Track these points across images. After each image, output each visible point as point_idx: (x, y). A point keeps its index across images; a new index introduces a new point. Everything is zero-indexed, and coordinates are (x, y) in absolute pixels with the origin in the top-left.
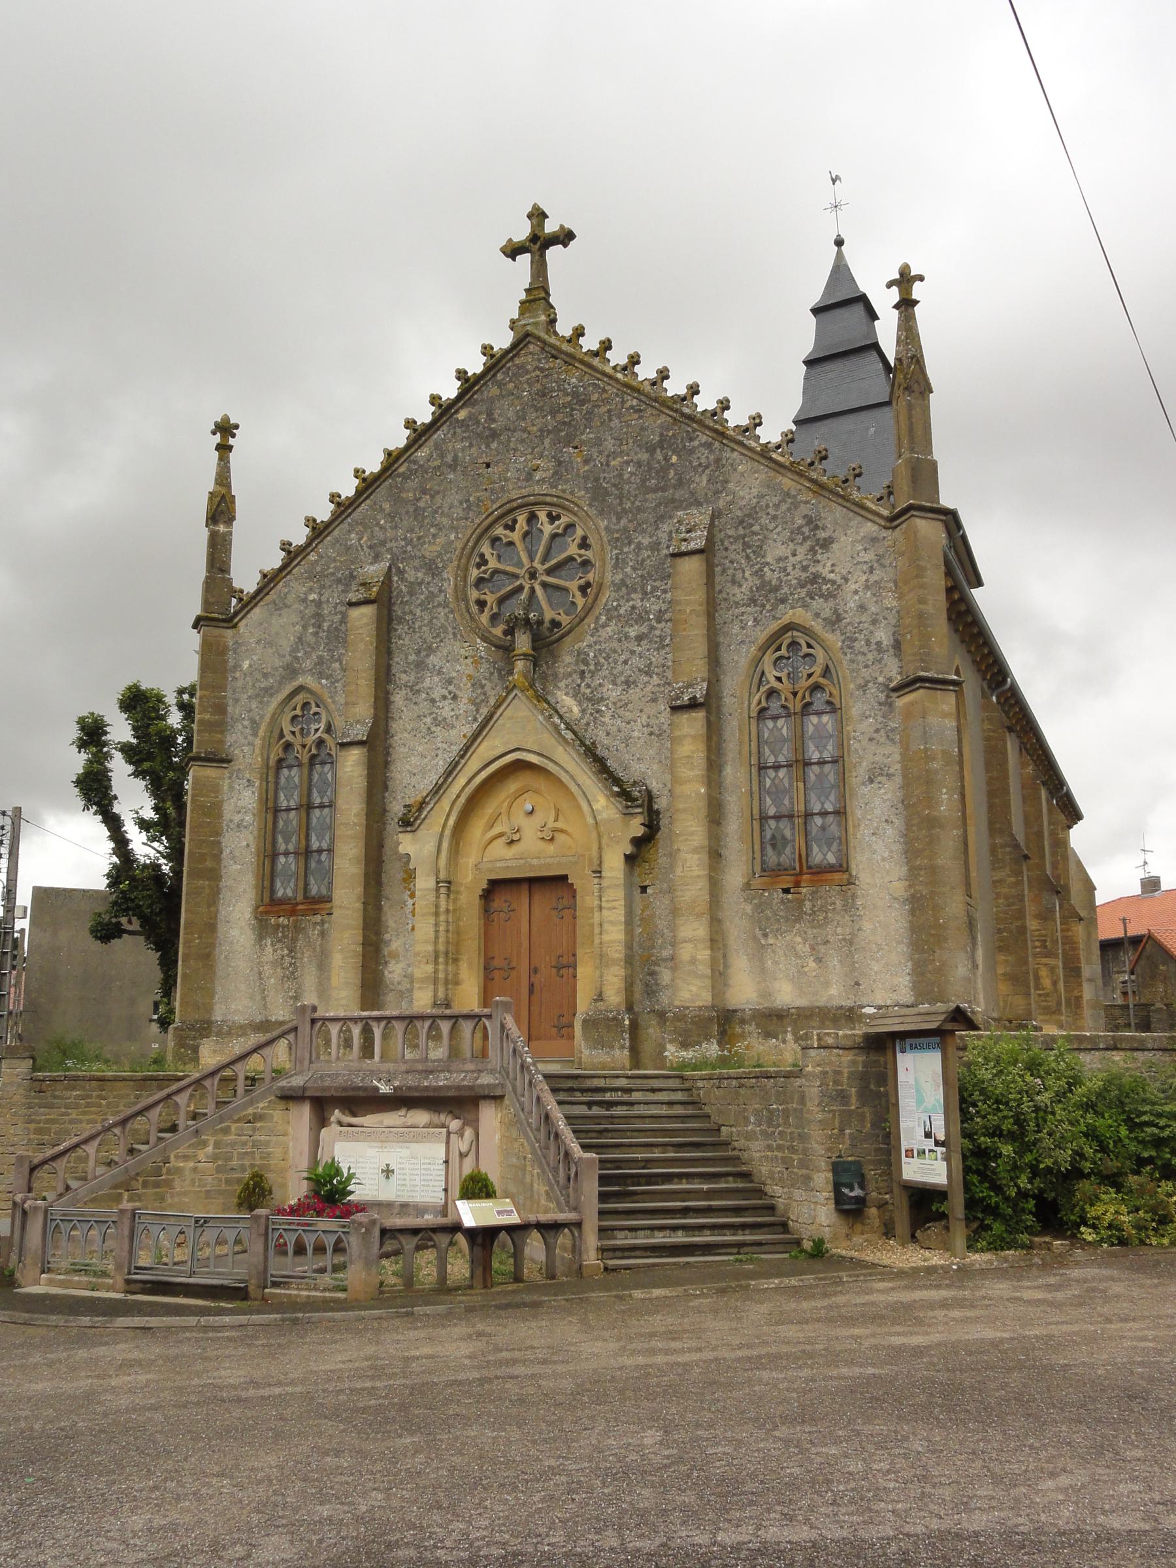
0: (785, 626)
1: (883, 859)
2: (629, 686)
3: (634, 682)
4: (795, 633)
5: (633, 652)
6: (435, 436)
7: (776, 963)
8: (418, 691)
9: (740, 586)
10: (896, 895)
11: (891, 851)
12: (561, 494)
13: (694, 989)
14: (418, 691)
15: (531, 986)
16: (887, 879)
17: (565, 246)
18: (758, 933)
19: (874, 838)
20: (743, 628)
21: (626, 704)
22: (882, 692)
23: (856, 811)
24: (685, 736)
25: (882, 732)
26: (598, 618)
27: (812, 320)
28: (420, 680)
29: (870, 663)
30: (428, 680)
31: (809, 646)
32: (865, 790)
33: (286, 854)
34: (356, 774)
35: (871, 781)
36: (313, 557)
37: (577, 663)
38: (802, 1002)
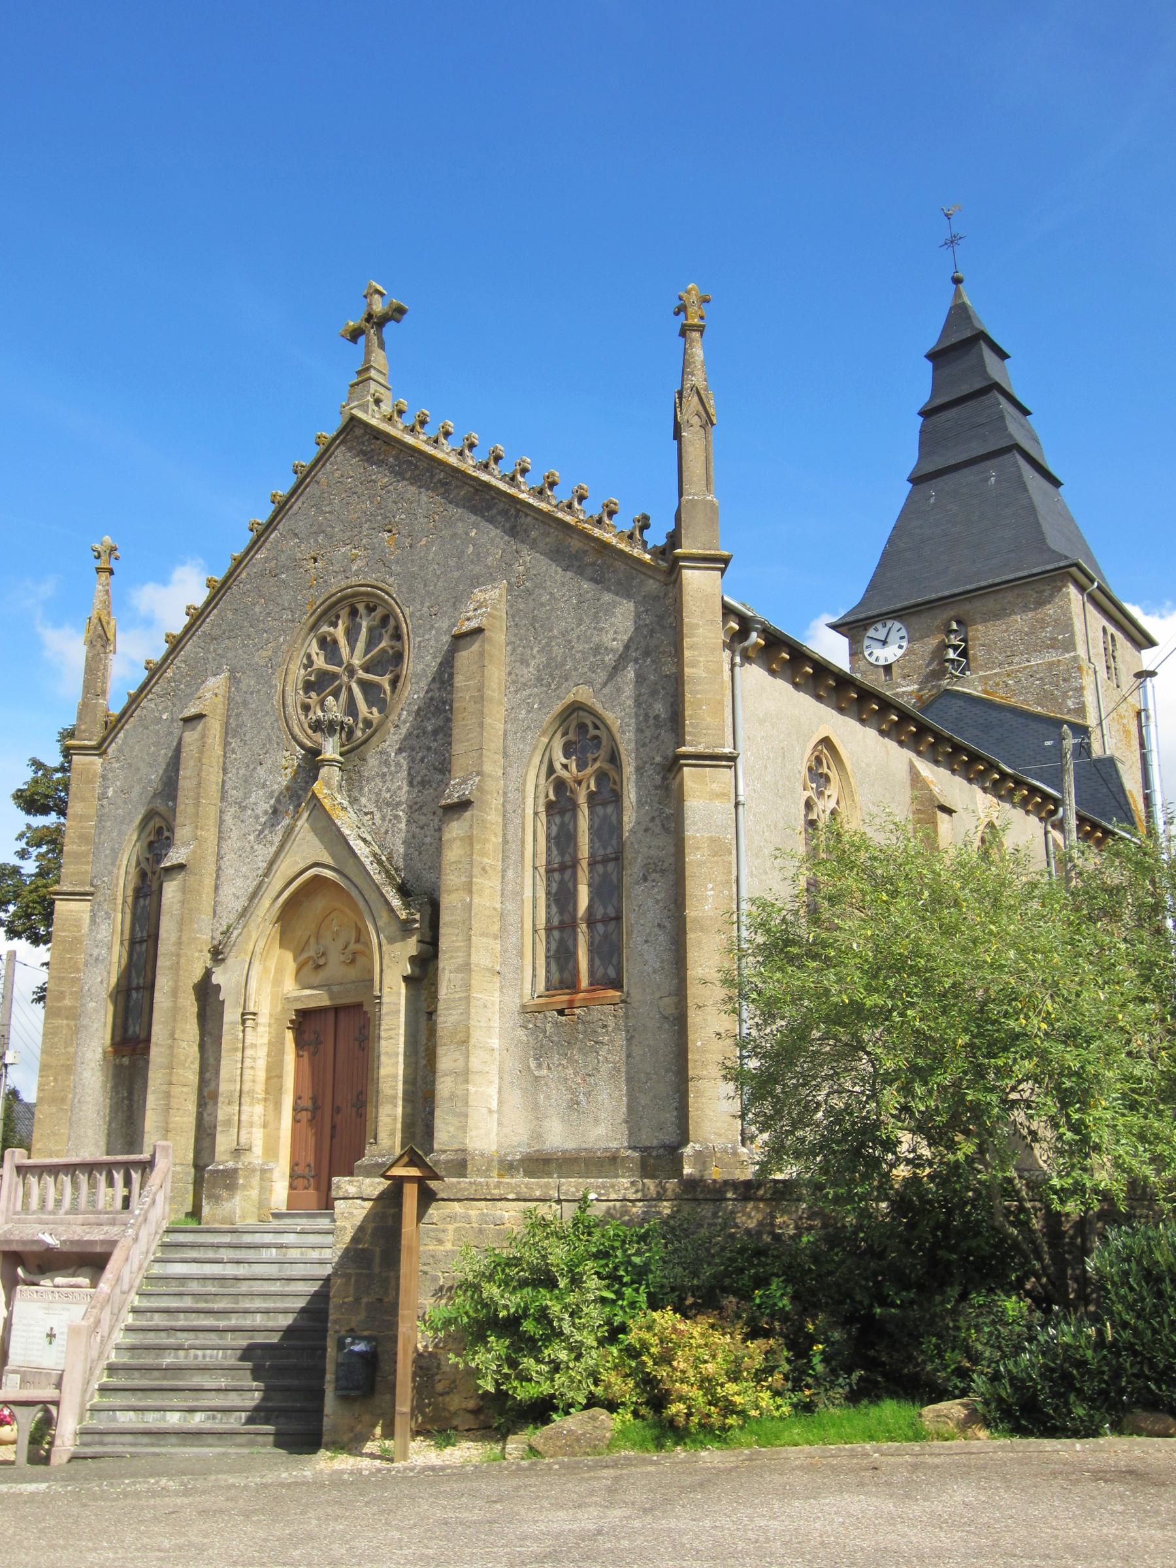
0: (569, 706)
1: (654, 972)
2: (424, 787)
3: (430, 782)
4: (581, 713)
5: (429, 749)
6: (273, 536)
7: (548, 1097)
8: (245, 807)
9: (528, 665)
10: (666, 1013)
11: (662, 962)
12: (375, 583)
13: (452, 1129)
14: (245, 807)
15: (333, 1127)
16: (657, 995)
17: (398, 321)
18: (532, 1064)
19: (645, 946)
20: (529, 712)
21: (421, 808)
22: (658, 774)
23: (630, 917)
24: (455, 839)
25: (657, 821)
26: (400, 715)
27: (929, 365)
28: (246, 796)
29: (647, 740)
30: (253, 795)
31: (596, 727)
32: (639, 889)
33: (138, 989)
34: (175, 900)
35: (645, 879)
36: (169, 674)
37: (380, 766)
38: (571, 1145)
